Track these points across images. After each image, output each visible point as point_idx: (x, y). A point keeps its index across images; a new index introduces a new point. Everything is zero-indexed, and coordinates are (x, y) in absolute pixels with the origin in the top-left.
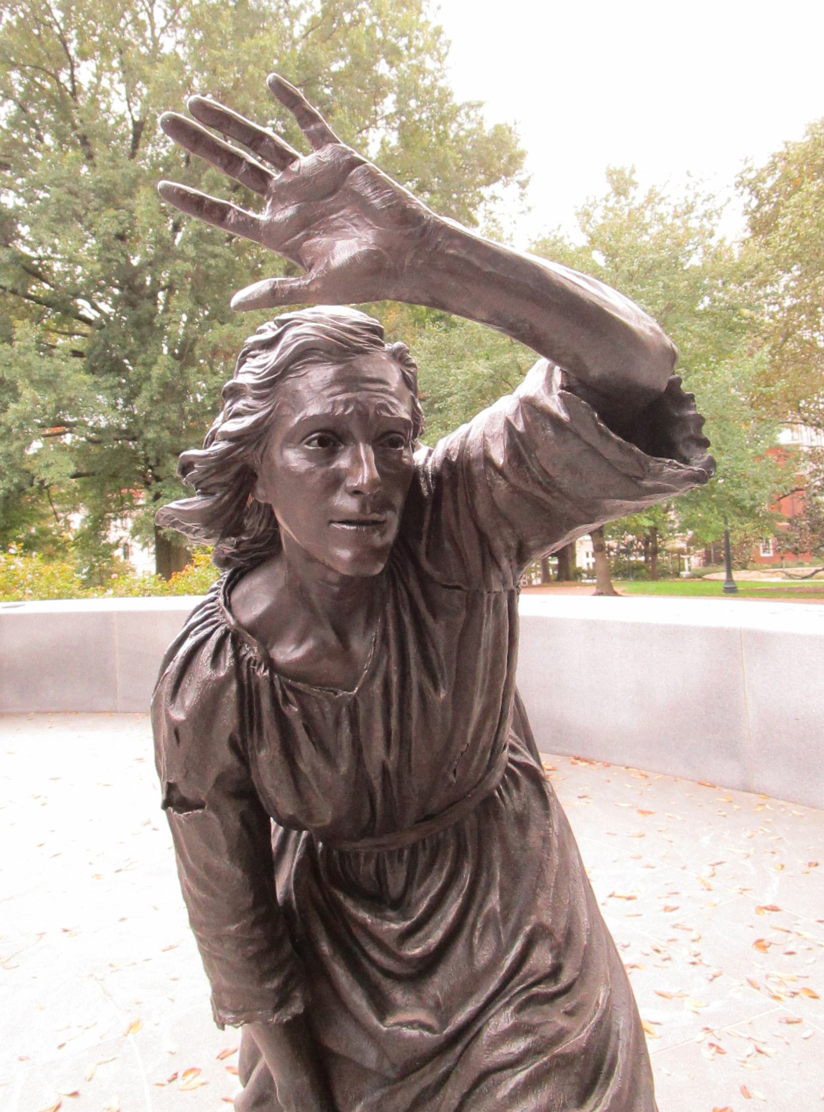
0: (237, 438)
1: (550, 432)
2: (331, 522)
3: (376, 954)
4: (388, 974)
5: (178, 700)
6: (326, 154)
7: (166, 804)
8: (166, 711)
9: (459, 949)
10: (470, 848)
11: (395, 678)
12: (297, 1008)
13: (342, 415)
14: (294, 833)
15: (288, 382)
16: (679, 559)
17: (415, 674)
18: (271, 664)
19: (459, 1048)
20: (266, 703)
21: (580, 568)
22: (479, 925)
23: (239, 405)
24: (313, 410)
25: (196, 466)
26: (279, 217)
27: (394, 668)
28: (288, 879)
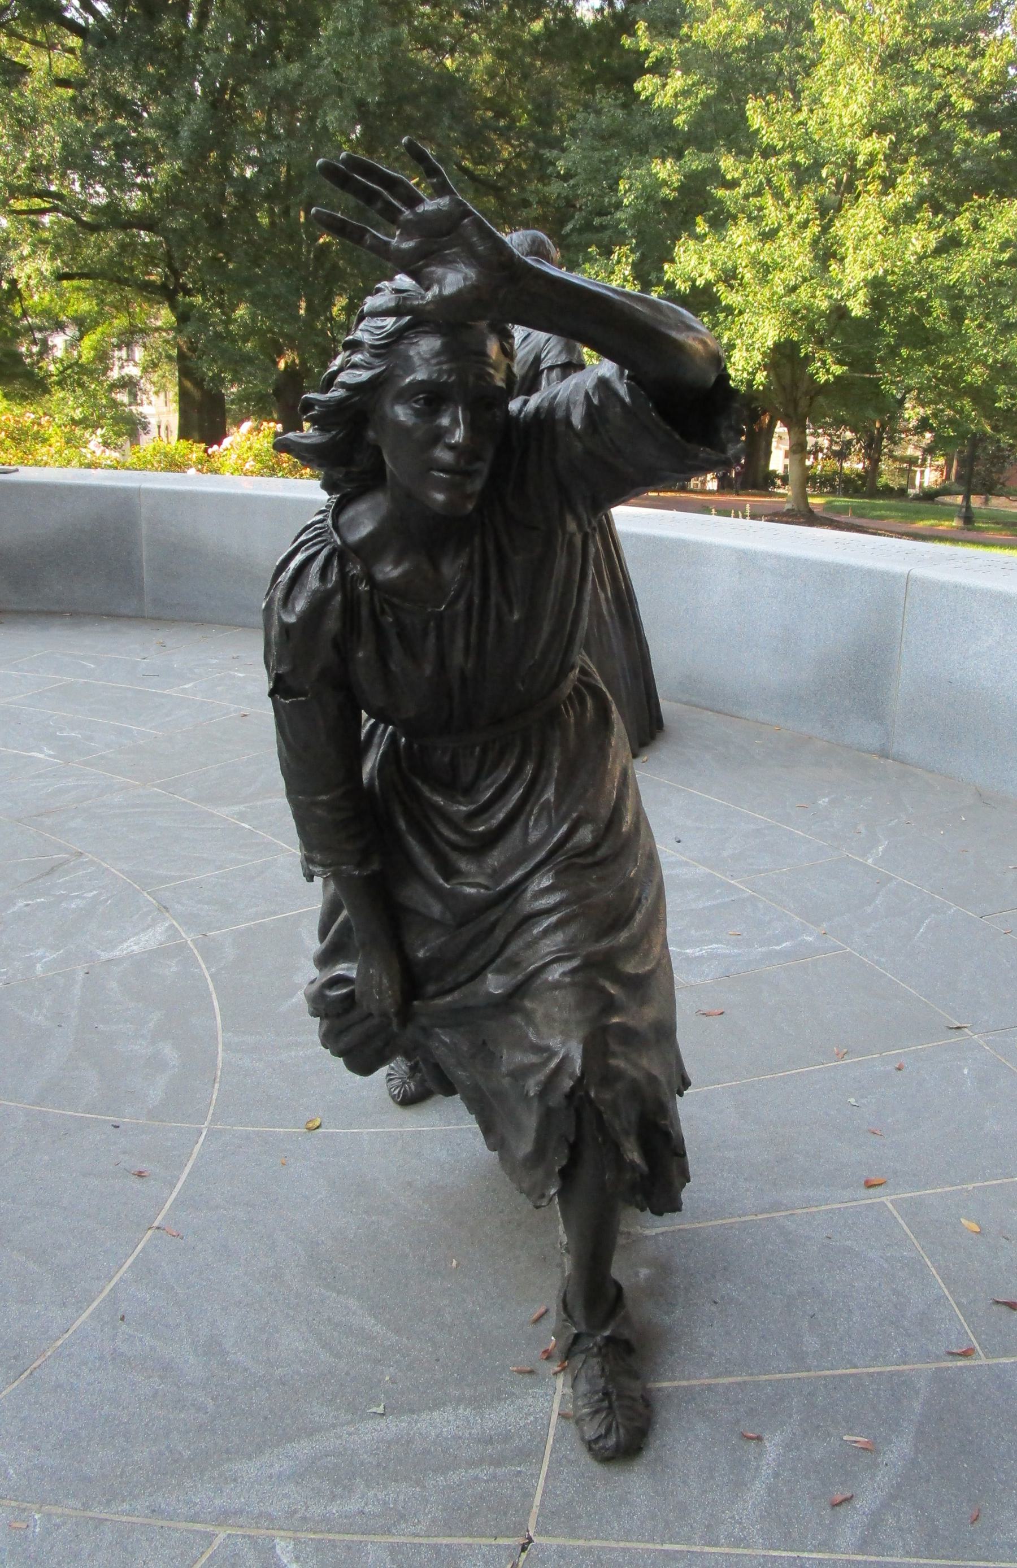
0: (354, 389)
1: (618, 409)
2: (432, 469)
3: (447, 832)
4: (455, 847)
5: (290, 606)
6: (444, 202)
7: (272, 694)
8: (278, 614)
9: (517, 832)
10: (534, 749)
11: (476, 600)
12: (375, 866)
13: (445, 383)
14: (382, 726)
15: (402, 347)
16: (910, 470)
17: (494, 598)
18: (371, 580)
19: (509, 901)
20: (365, 611)
21: (774, 472)
22: (535, 812)
23: (357, 358)
24: (421, 375)
25: (316, 408)
26: (405, 245)
27: (477, 591)
28: (374, 766)
